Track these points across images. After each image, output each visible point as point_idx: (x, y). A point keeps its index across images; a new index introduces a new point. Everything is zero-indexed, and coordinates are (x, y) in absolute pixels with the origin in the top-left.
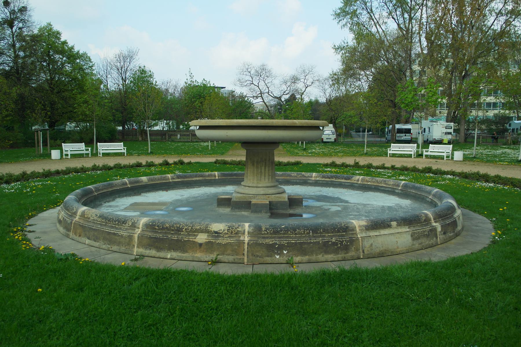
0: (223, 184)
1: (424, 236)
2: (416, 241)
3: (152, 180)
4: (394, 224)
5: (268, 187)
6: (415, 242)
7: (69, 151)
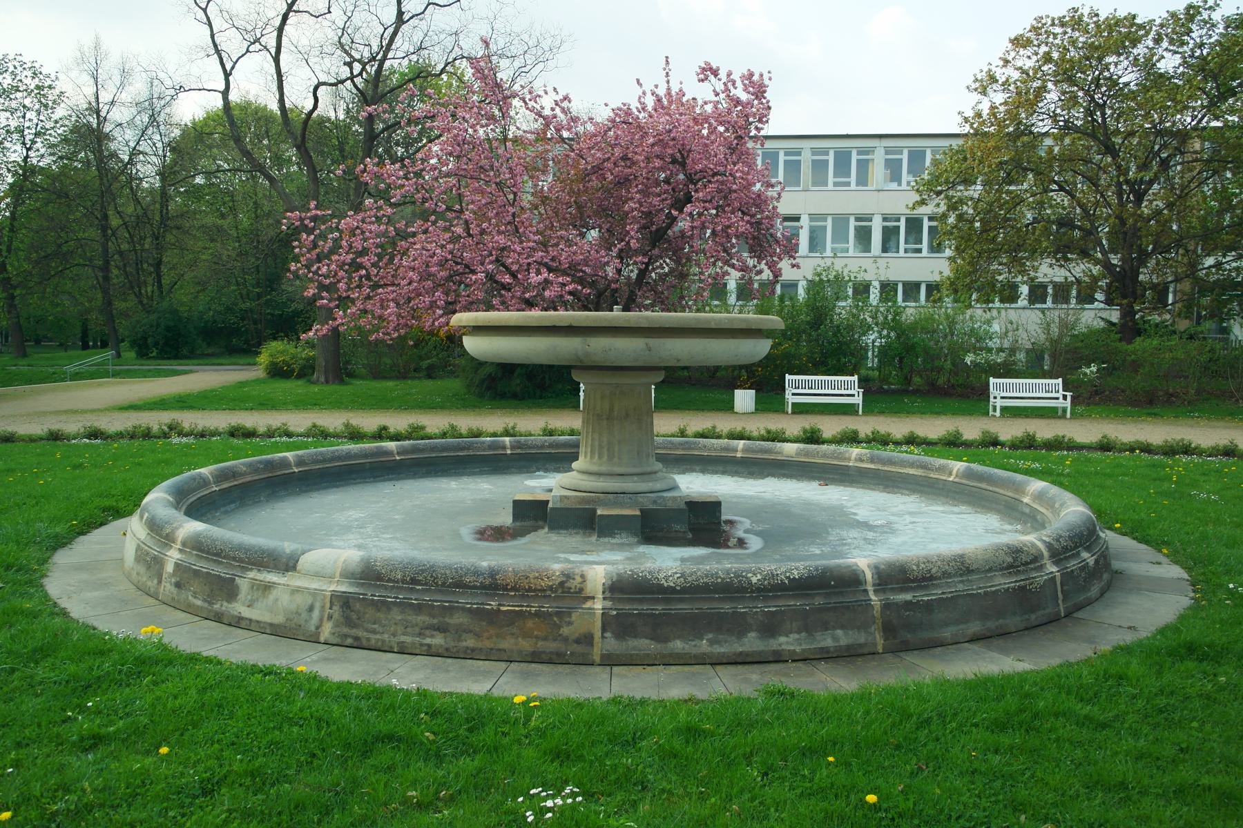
0: (954, 499)
3: (807, 454)
5: (590, 473)
7: (999, 398)
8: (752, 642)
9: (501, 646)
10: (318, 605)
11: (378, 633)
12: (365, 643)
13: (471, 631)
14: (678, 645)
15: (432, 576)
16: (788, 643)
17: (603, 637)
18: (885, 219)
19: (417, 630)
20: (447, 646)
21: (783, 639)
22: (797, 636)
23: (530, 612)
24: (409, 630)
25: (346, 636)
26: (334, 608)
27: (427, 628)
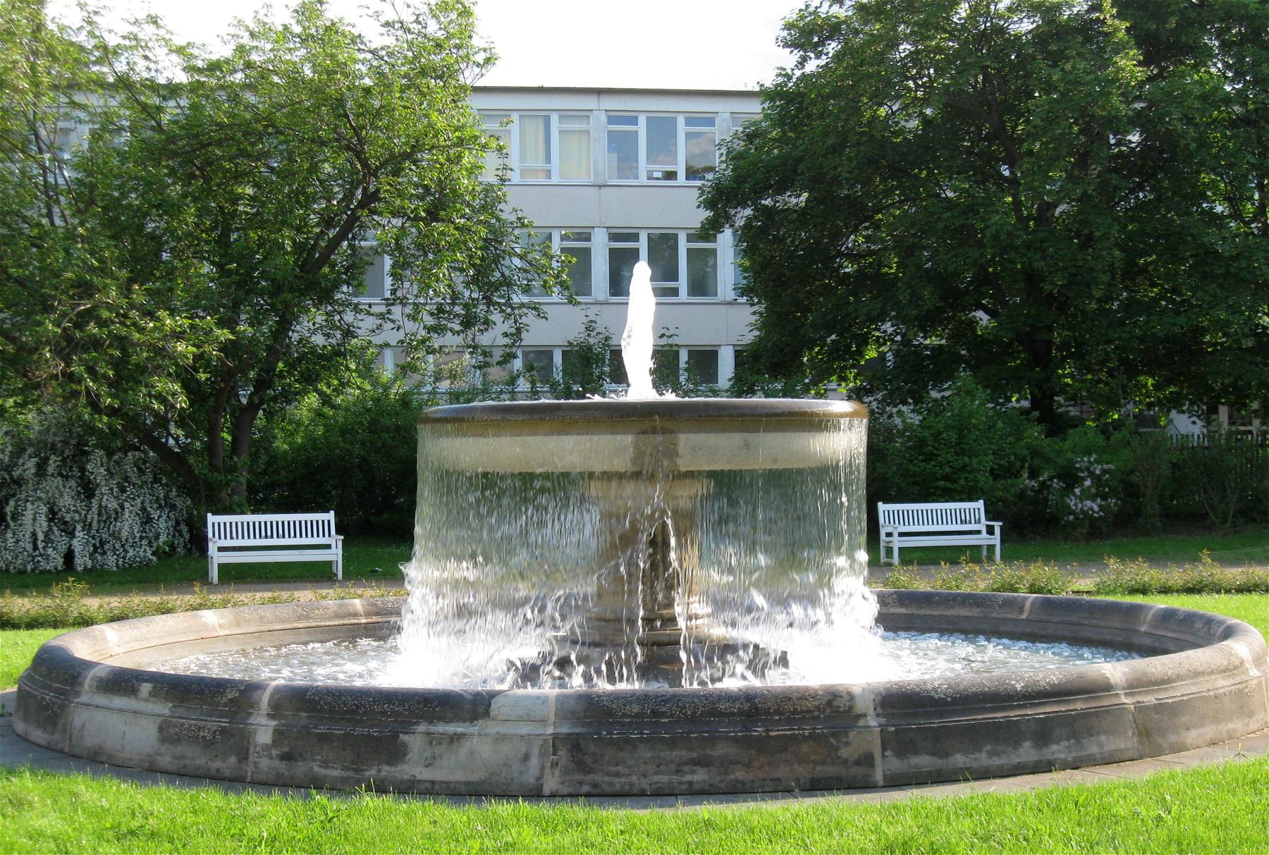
1: (196, 740)
2: (167, 745)
4: (146, 688)
6: (163, 749)
7: (896, 535)
8: (1027, 752)
9: (775, 775)
10: (535, 752)
11: (624, 775)
12: (607, 788)
13: (738, 763)
14: (959, 760)
15: (678, 706)
16: (1060, 752)
17: (884, 756)
18: (614, 237)
19: (673, 767)
20: (711, 781)
21: (1054, 747)
22: (1066, 743)
23: (803, 735)
24: (663, 768)
25: (581, 783)
26: (560, 753)
27: (686, 764)
